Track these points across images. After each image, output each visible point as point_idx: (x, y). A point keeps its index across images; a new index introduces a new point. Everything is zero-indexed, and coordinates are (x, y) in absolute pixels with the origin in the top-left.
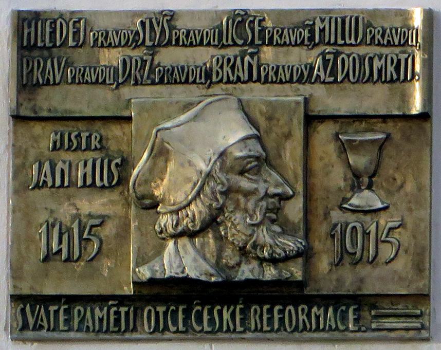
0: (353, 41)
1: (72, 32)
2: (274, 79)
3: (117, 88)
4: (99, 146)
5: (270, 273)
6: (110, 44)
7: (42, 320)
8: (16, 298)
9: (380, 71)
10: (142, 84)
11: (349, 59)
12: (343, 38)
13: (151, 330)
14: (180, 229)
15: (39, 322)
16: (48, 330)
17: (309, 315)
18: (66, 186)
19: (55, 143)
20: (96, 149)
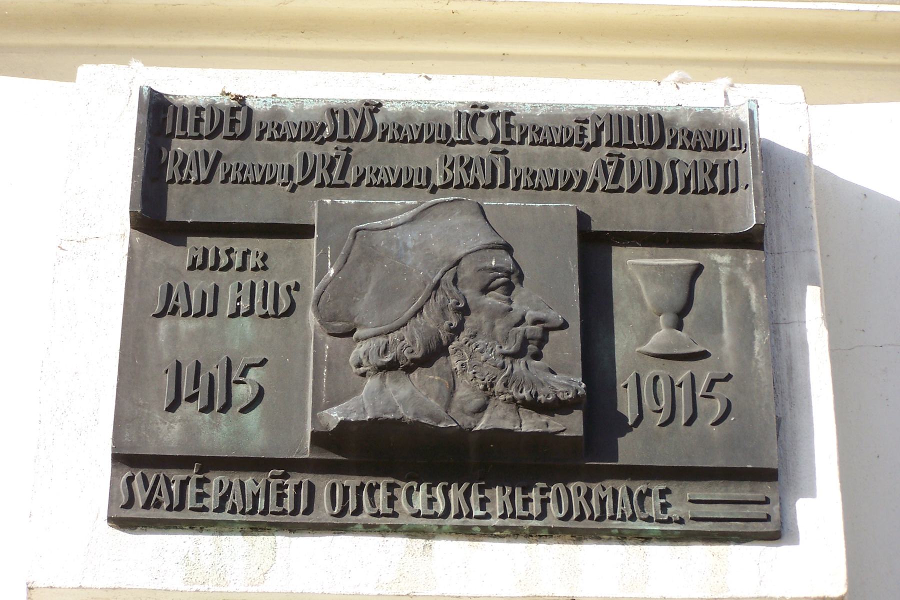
0: (645, 141)
1: (275, 497)
2: (530, 184)
3: (293, 190)
4: (260, 265)
5: (530, 423)
6: (284, 136)
7: (160, 494)
8: (121, 459)
9: (687, 179)
10: (330, 185)
11: (633, 512)
12: (631, 137)
13: (336, 512)
14: (388, 359)
15: (156, 495)
16: (169, 509)
17: (588, 496)
18: (208, 308)
19: (195, 260)
20: (256, 269)
